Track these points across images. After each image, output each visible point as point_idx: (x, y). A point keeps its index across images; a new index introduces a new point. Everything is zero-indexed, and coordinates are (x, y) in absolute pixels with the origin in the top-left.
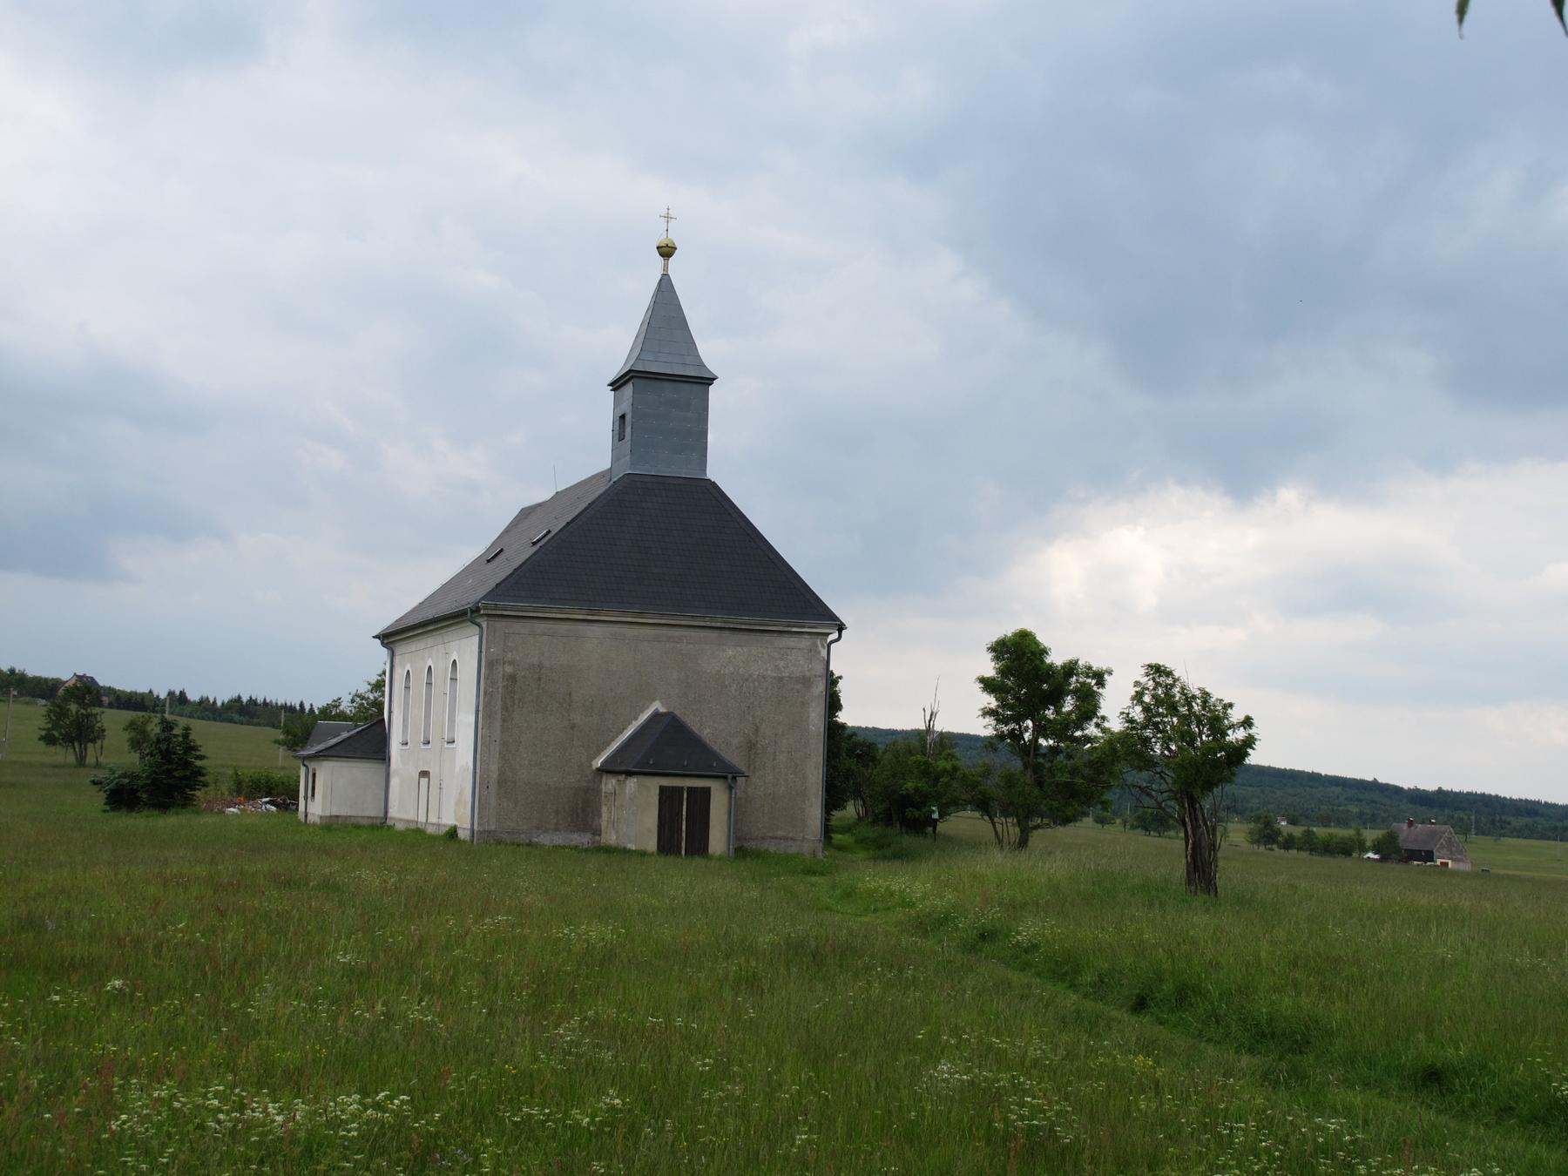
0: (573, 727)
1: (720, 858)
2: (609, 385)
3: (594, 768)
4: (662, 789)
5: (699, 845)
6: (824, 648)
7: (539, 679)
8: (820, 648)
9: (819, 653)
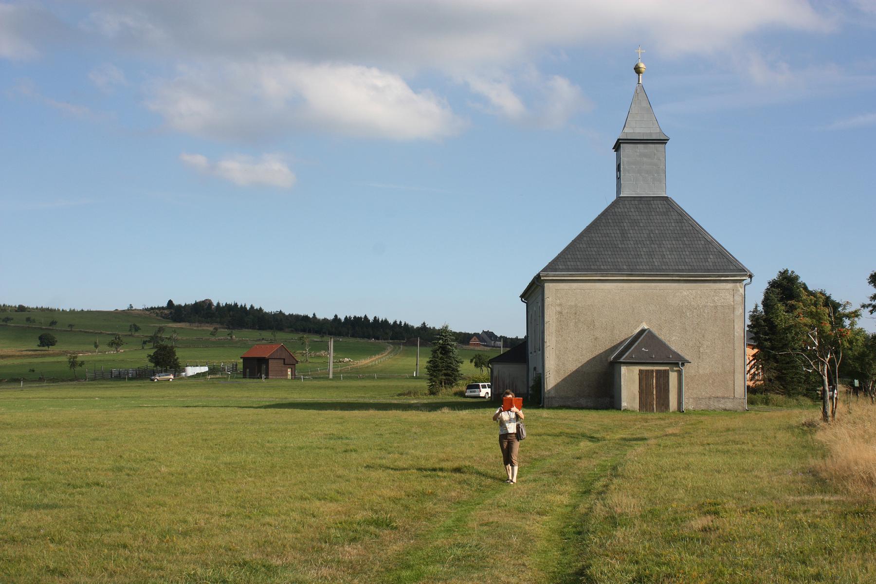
0: (596, 339)
1: (674, 412)
2: (613, 149)
3: (609, 361)
4: (641, 371)
5: (664, 404)
6: (742, 288)
7: (576, 314)
8: (740, 289)
9: (739, 290)
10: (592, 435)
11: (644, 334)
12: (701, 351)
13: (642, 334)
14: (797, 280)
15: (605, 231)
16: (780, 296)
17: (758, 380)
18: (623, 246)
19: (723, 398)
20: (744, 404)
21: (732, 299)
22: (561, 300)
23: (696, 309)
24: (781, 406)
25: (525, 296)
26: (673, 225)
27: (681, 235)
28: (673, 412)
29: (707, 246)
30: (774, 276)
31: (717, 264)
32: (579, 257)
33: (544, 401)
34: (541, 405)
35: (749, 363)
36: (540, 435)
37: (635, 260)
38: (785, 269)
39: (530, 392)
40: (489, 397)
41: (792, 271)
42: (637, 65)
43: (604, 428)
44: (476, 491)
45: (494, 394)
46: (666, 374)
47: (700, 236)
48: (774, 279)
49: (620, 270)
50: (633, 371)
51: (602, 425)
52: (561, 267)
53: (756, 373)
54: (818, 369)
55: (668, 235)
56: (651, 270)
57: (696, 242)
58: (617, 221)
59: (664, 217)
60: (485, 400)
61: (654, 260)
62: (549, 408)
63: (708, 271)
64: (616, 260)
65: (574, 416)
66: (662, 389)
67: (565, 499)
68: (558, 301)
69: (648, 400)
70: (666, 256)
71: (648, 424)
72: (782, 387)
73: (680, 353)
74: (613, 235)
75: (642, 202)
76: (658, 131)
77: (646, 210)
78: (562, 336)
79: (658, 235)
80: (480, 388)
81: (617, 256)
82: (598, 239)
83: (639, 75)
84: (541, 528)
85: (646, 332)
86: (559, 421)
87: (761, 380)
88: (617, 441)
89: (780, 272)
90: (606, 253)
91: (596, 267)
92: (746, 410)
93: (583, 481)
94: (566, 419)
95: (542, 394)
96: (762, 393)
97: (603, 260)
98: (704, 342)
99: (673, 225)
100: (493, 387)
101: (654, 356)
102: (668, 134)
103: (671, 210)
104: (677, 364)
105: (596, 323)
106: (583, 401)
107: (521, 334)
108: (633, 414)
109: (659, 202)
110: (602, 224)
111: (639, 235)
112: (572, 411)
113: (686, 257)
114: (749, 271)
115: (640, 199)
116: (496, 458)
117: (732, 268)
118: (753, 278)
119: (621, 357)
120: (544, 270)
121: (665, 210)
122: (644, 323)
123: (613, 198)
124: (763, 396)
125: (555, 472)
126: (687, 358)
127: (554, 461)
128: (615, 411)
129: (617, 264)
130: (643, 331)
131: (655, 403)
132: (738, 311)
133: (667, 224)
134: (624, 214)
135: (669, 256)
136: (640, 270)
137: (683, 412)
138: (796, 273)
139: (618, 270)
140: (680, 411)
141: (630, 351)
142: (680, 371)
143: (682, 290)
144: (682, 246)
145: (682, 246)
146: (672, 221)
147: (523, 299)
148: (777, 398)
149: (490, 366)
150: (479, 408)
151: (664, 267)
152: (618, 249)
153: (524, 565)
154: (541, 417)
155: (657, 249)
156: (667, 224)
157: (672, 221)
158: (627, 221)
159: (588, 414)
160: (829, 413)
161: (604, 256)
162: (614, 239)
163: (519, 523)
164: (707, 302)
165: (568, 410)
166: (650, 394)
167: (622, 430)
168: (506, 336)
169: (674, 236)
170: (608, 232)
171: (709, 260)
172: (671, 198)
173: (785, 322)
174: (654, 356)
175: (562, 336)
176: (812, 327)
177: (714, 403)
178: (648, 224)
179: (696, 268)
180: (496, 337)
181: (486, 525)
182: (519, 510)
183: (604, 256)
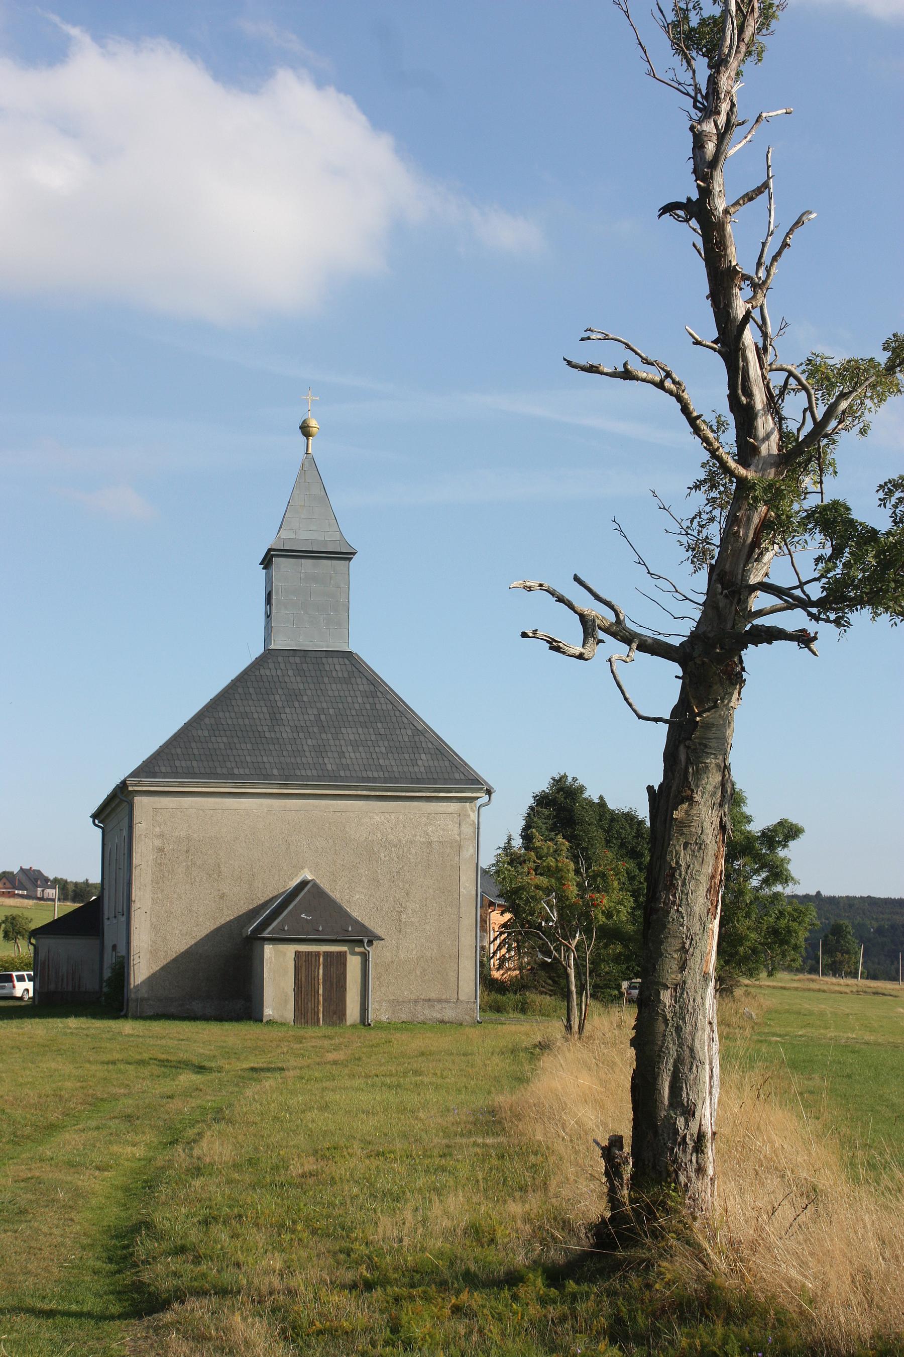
0: (222, 897)
1: (353, 1026)
3: (244, 935)
4: (298, 954)
5: (337, 1012)
6: (474, 812)
7: (187, 851)
8: (471, 813)
10: (203, 1064)
11: (306, 889)
12: (403, 920)
13: (302, 889)
14: (582, 793)
15: (242, 709)
16: (551, 822)
17: (509, 969)
18: (273, 735)
19: (439, 1001)
20: (473, 1011)
21: (456, 830)
22: (162, 827)
23: (396, 846)
24: (548, 1016)
25: (101, 815)
26: (360, 700)
27: (372, 719)
28: (350, 1026)
29: (417, 738)
30: (543, 785)
31: (433, 769)
32: (196, 752)
33: (128, 1005)
34: (122, 1013)
35: (495, 939)
36: (114, 1063)
37: (293, 760)
38: (562, 774)
39: (105, 990)
40: (29, 998)
41: (574, 778)
42: (304, 422)
43: (226, 1052)
44: (8, 1143)
45: (39, 993)
46: (341, 958)
47: (405, 720)
48: (544, 791)
49: (266, 777)
50: (285, 954)
51: (223, 1047)
52: (163, 769)
53: (507, 956)
54: (560, 957)
55: (350, 718)
56: (319, 778)
57: (398, 731)
58: (263, 691)
59: (344, 686)
60: (23, 1004)
61: (326, 760)
62: (136, 1017)
63: (418, 781)
64: (260, 759)
65: (178, 1033)
66: (335, 986)
67: (140, 1152)
68: (157, 829)
69: (309, 1003)
70: (347, 755)
71: (301, 1045)
72: (550, 982)
73: (366, 924)
74: (256, 716)
75: (308, 660)
76: (338, 538)
77: (313, 674)
78: (162, 891)
79: (334, 718)
80: (12, 981)
81: (263, 753)
82: (230, 722)
83: (308, 439)
84: (100, 1185)
85: (309, 886)
86: (152, 1042)
87: (515, 970)
88: (240, 1073)
89: (553, 779)
90: (243, 746)
91: (225, 771)
92: (478, 1022)
93: (170, 1128)
94: (165, 1037)
95: (125, 991)
96: (516, 993)
97: (238, 759)
98: (408, 904)
99: (360, 700)
100: (38, 980)
101: (321, 929)
102: (354, 541)
103: (356, 674)
104: (360, 942)
105: (223, 869)
106: (196, 1007)
107: (95, 877)
108: (283, 1028)
109: (336, 660)
110: (237, 696)
111: (301, 717)
112: (177, 1023)
113: (380, 756)
114: (486, 783)
115: (305, 653)
116: (40, 1097)
117: (457, 776)
118: (493, 795)
119: (264, 930)
120: (134, 774)
121: (346, 675)
122: (306, 870)
123: (259, 650)
124: (518, 997)
125: (129, 1116)
126: (378, 931)
127: (130, 1102)
128: (252, 1023)
129: (261, 766)
130: (304, 884)
131: (321, 1009)
132: (467, 851)
133: (349, 699)
134: (276, 679)
135: (352, 755)
136: (303, 777)
137: (370, 1025)
138: (581, 781)
139: (265, 776)
140: (364, 1025)
141: (281, 918)
142: (365, 953)
143: (372, 814)
144: (373, 737)
145: (373, 737)
146: (358, 694)
147: (97, 822)
148: (542, 1001)
149: (33, 941)
150: (11, 1018)
151: (342, 773)
152: (264, 741)
153: (72, 1220)
154: (120, 1033)
155: (332, 742)
156: (349, 699)
157: (358, 694)
158: (280, 691)
159: (205, 1029)
160: (576, 1027)
161: (240, 752)
162: (258, 722)
163: (69, 1178)
164: (415, 835)
165: (169, 1022)
166: (313, 994)
167: (256, 1055)
168: (65, 878)
169: (361, 719)
170: (247, 709)
171: (420, 762)
172: (356, 654)
173: (511, 882)
174: (321, 929)
175: (162, 891)
176: (548, 891)
177: (423, 1009)
178: (316, 699)
179: (397, 775)
180: (47, 880)
181: (23, 1181)
182: (71, 1164)
183: (240, 752)
